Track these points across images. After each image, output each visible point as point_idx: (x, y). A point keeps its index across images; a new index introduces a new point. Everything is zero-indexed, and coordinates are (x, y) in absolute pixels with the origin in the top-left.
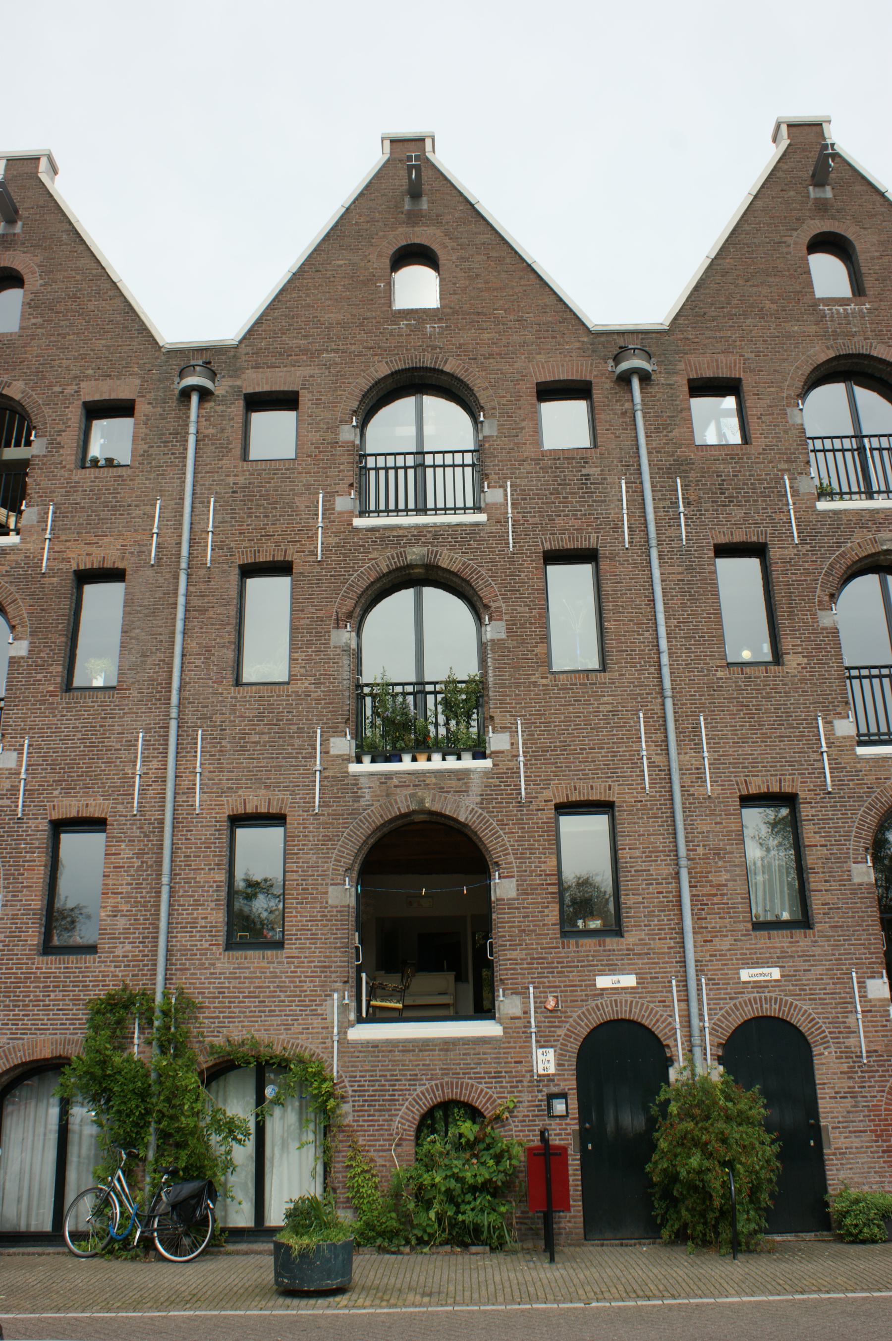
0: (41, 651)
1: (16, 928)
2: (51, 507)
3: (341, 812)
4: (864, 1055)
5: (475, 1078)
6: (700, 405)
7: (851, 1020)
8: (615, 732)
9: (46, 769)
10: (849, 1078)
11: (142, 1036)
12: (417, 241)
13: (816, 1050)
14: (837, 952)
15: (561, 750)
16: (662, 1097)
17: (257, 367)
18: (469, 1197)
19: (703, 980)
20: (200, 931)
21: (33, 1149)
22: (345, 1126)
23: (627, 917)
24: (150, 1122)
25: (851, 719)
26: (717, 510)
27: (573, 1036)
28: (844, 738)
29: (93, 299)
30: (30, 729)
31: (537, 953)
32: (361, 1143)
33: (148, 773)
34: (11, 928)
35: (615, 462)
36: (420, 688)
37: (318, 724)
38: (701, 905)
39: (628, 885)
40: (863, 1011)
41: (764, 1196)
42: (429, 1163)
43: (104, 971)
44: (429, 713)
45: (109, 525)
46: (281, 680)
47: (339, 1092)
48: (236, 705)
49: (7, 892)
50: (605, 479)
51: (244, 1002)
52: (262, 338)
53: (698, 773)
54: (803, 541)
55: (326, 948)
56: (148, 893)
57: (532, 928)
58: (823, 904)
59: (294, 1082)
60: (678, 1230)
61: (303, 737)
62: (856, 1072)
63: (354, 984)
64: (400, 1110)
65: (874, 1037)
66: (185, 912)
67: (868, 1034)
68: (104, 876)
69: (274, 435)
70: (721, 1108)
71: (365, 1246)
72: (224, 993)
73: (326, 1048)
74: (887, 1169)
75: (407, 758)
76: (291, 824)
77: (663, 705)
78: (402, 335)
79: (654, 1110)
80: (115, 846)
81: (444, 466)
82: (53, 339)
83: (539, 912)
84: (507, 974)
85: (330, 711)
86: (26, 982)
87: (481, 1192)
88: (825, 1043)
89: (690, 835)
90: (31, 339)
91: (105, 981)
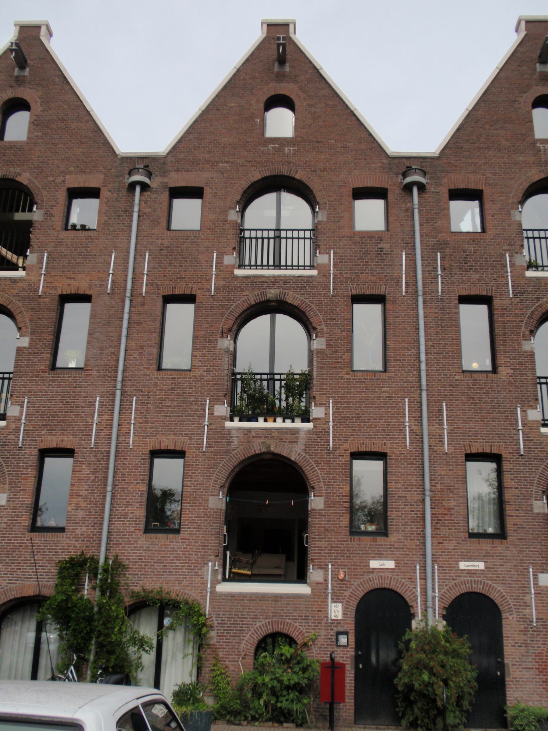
0: (37, 344)
1: (15, 515)
2: (46, 254)
3: (219, 451)
4: (535, 620)
5: (293, 619)
6: (456, 205)
7: (527, 598)
8: (390, 410)
9: (38, 417)
10: (525, 634)
11: (90, 584)
12: (282, 92)
13: (504, 616)
14: (521, 555)
15: (356, 420)
16: (406, 637)
17: (178, 170)
18: (285, 693)
19: (436, 567)
20: (129, 521)
21: (18, 651)
22: (212, 645)
23: (391, 525)
24: (92, 637)
25: (538, 410)
26: (462, 274)
27: (354, 596)
28: (533, 421)
29: (74, 121)
30: (29, 392)
31: (335, 544)
32: (221, 655)
33: (101, 422)
34: (12, 515)
35: (399, 241)
36: (271, 377)
37: (207, 396)
38: (438, 520)
39: (392, 505)
40: (535, 593)
41: (466, 704)
42: (261, 669)
43: (68, 544)
44: (276, 393)
45: (82, 267)
46: (186, 368)
47: (209, 623)
48: (157, 383)
49: (11, 492)
50: (392, 251)
51: (154, 566)
52: (181, 152)
53: (440, 438)
54: (515, 296)
55: (206, 534)
56: (98, 496)
57: (332, 528)
58: (514, 525)
59: (182, 616)
60: (412, 721)
61: (198, 404)
62: (529, 631)
63: (222, 558)
64: (245, 636)
65: (541, 609)
66: (120, 509)
67: (538, 608)
68: (71, 485)
69: (187, 214)
70: (443, 647)
71: (219, 719)
72: (142, 559)
73: (203, 596)
74: (544, 693)
75: (261, 419)
76: (188, 457)
77: (421, 394)
78: (270, 154)
79: (401, 646)
80: (79, 466)
81: (298, 238)
82: (48, 146)
83: (337, 519)
84: (315, 556)
85: (215, 389)
86: (19, 549)
87: (292, 690)
88: (510, 611)
89: (433, 476)
90: (35, 146)
91: (69, 549)
